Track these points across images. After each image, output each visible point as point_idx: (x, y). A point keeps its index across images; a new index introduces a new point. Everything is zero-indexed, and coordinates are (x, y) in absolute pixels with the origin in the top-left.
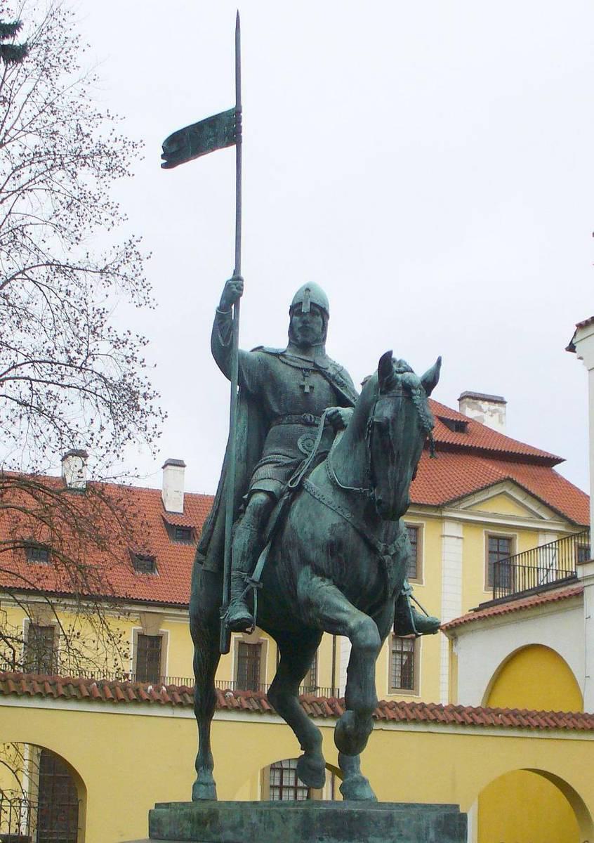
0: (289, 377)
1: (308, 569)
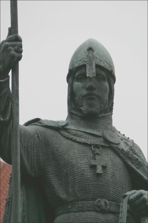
0: (78, 158)
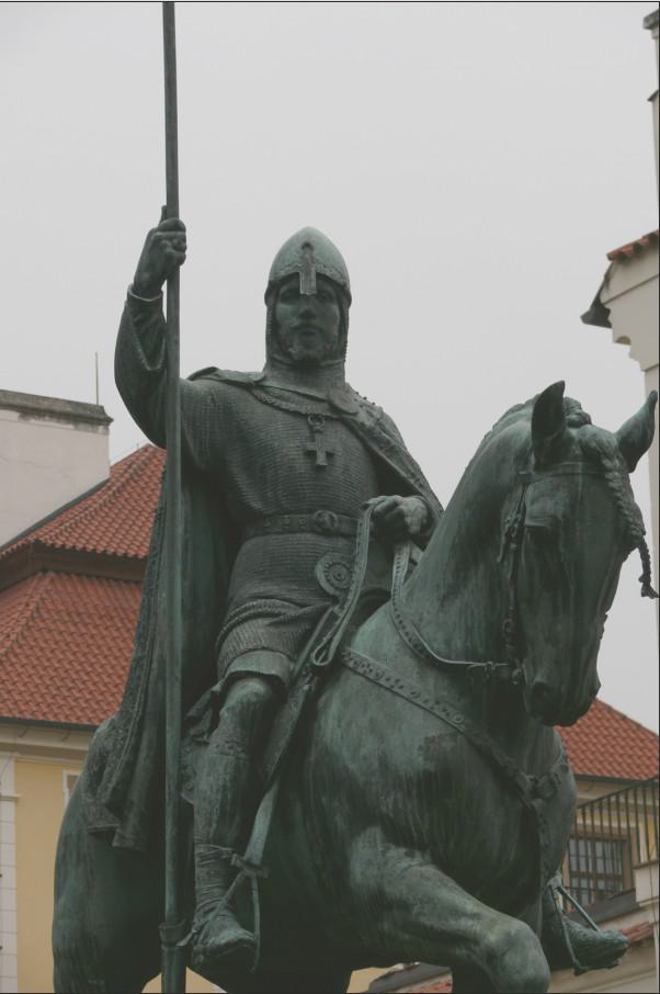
0: (283, 438)
1: (376, 832)
